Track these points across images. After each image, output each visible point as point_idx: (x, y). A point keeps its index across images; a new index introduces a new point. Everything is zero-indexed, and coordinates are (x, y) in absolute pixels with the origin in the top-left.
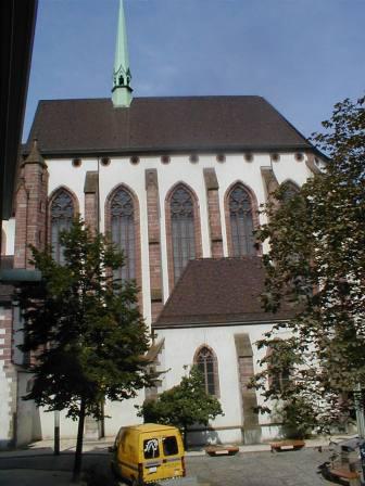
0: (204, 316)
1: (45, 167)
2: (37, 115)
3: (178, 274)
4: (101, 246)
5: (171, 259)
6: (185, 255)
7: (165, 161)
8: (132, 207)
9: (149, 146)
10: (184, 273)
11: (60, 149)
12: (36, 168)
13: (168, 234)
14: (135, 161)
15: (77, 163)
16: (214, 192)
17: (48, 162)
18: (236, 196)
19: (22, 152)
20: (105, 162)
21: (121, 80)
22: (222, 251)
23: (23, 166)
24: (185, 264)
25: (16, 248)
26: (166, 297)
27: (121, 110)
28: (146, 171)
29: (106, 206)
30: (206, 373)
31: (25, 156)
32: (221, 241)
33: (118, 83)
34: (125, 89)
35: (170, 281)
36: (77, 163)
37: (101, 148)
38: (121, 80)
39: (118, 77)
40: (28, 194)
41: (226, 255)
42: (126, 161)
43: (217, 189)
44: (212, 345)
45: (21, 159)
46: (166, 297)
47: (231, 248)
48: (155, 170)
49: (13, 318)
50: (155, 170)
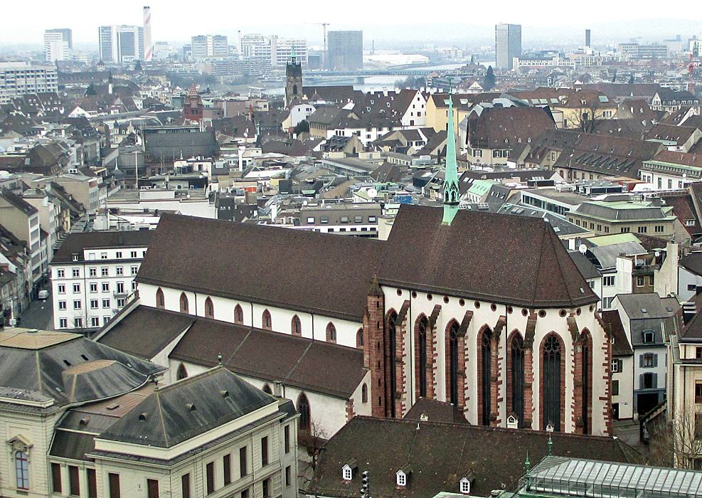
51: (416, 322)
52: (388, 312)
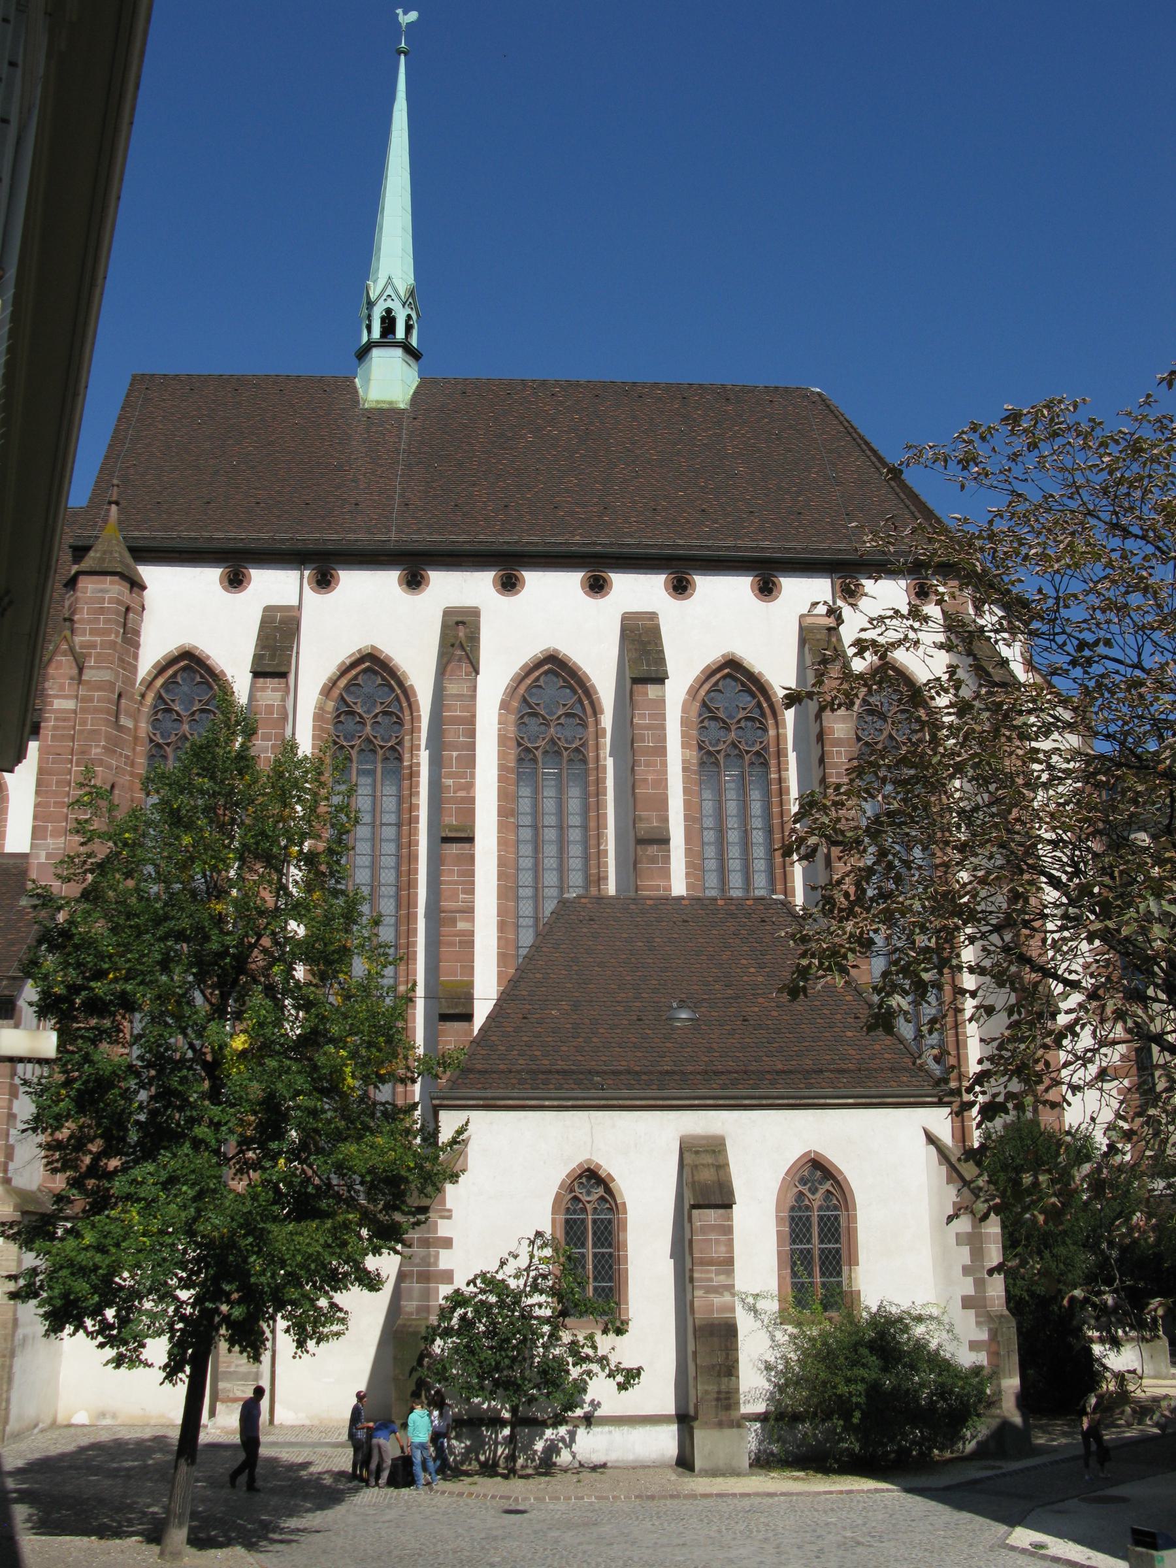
0: (709, 1075)
1: (137, 585)
2: (117, 439)
3: (527, 938)
4: (265, 868)
5: (507, 891)
6: (551, 878)
7: (509, 585)
8: (400, 723)
9: (460, 539)
10: (544, 934)
11: (186, 533)
12: (113, 588)
13: (503, 812)
14: (414, 582)
15: (235, 581)
16: (652, 690)
17: (149, 573)
18: (721, 704)
19: (68, 536)
20: (324, 582)
21: (389, 322)
22: (666, 873)
23: (72, 583)
24: (549, 907)
25: (37, 833)
26: (482, 1011)
27: (386, 415)
28: (448, 613)
29: (318, 717)
30: (590, 1250)
31: (80, 552)
32: (665, 841)
33: (376, 333)
34: (399, 352)
35: (502, 958)
36: (235, 581)
37: (311, 536)
38: (389, 322)
39: (378, 313)
40: (81, 670)
41: (679, 886)
42: (389, 579)
43: (660, 680)
44: (610, 1166)
45: (66, 556)
46: (482, 1011)
47: (695, 867)
48: (475, 613)
49: (634, 827)
50: (475, 613)
51: (327, 691)
52: (161, 669)
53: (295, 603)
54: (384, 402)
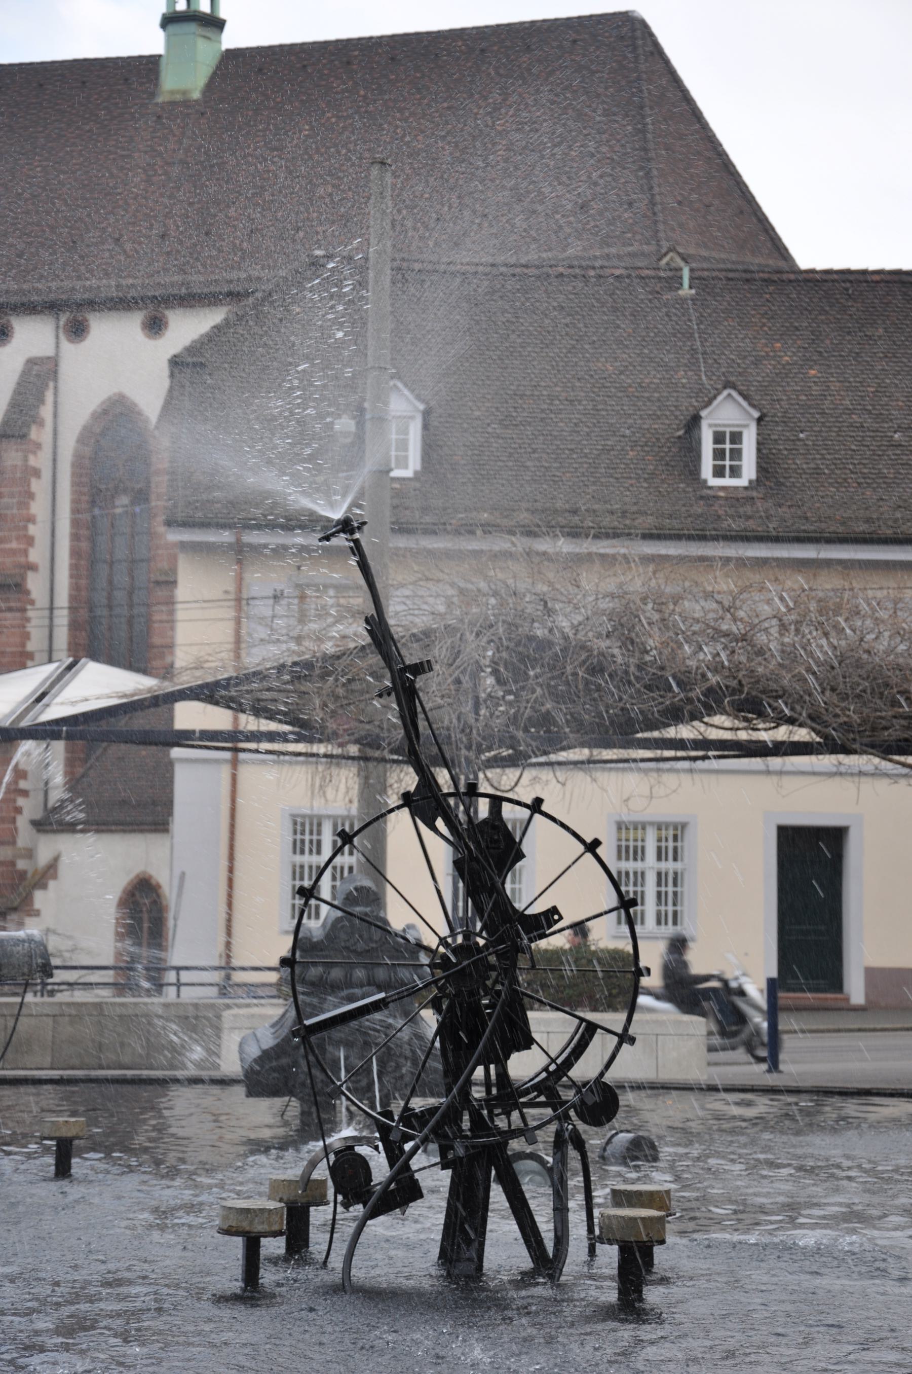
20: (78, 330)
27: (485, 821)
51: (81, 440)
53: (50, 352)
54: (178, 92)
